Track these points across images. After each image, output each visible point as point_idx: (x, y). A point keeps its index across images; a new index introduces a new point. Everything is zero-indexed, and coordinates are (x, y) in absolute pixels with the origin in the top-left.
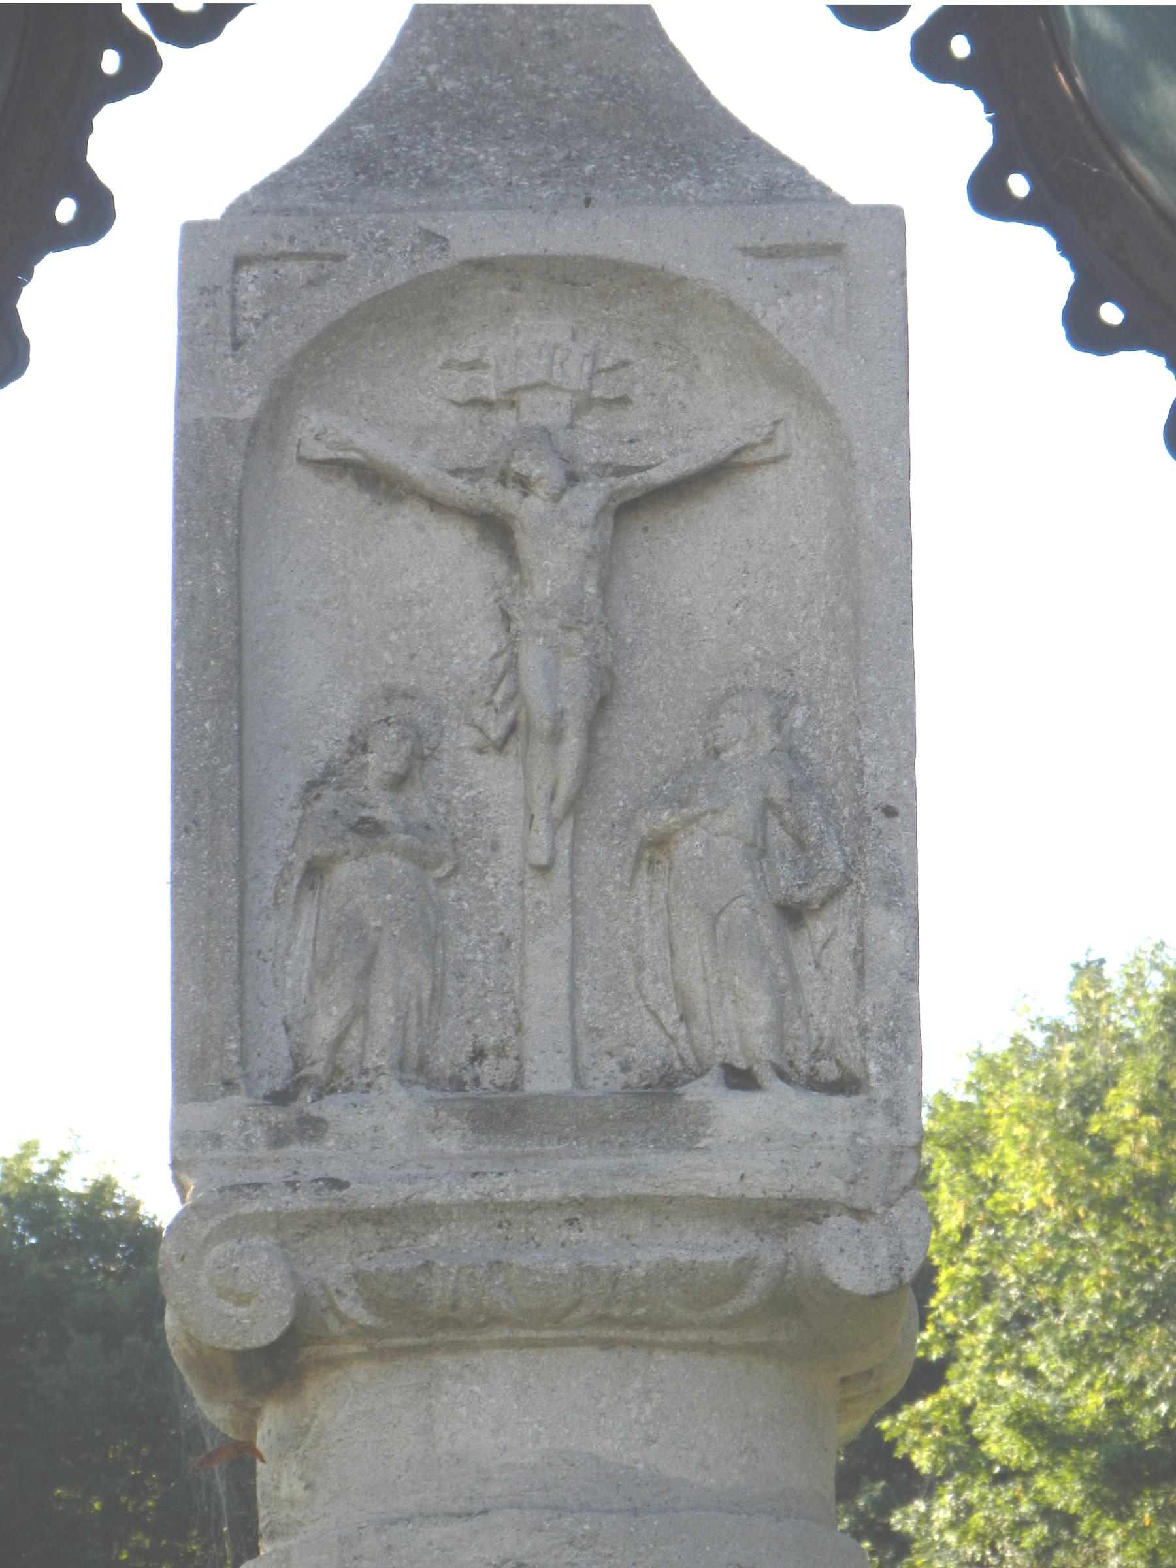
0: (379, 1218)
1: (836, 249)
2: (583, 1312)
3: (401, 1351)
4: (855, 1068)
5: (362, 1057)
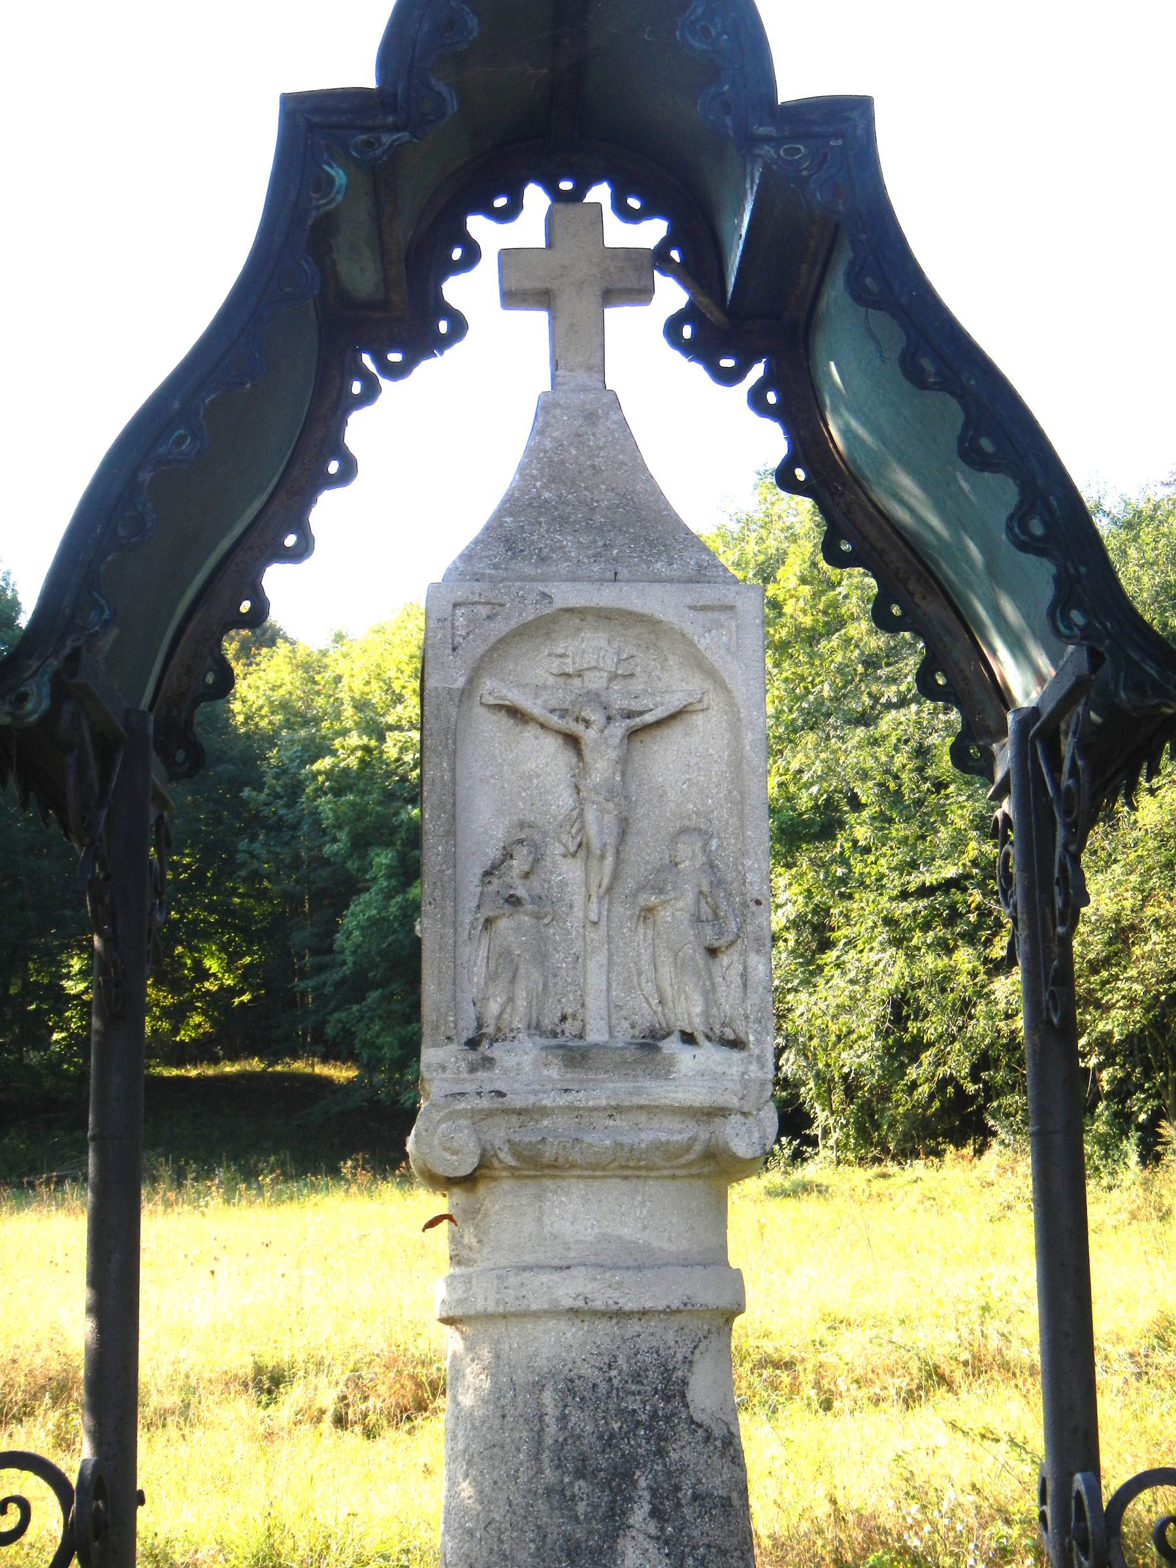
0: (520, 1112)
1: (732, 608)
2: (616, 1164)
3: (526, 1177)
4: (742, 1035)
5: (510, 1022)
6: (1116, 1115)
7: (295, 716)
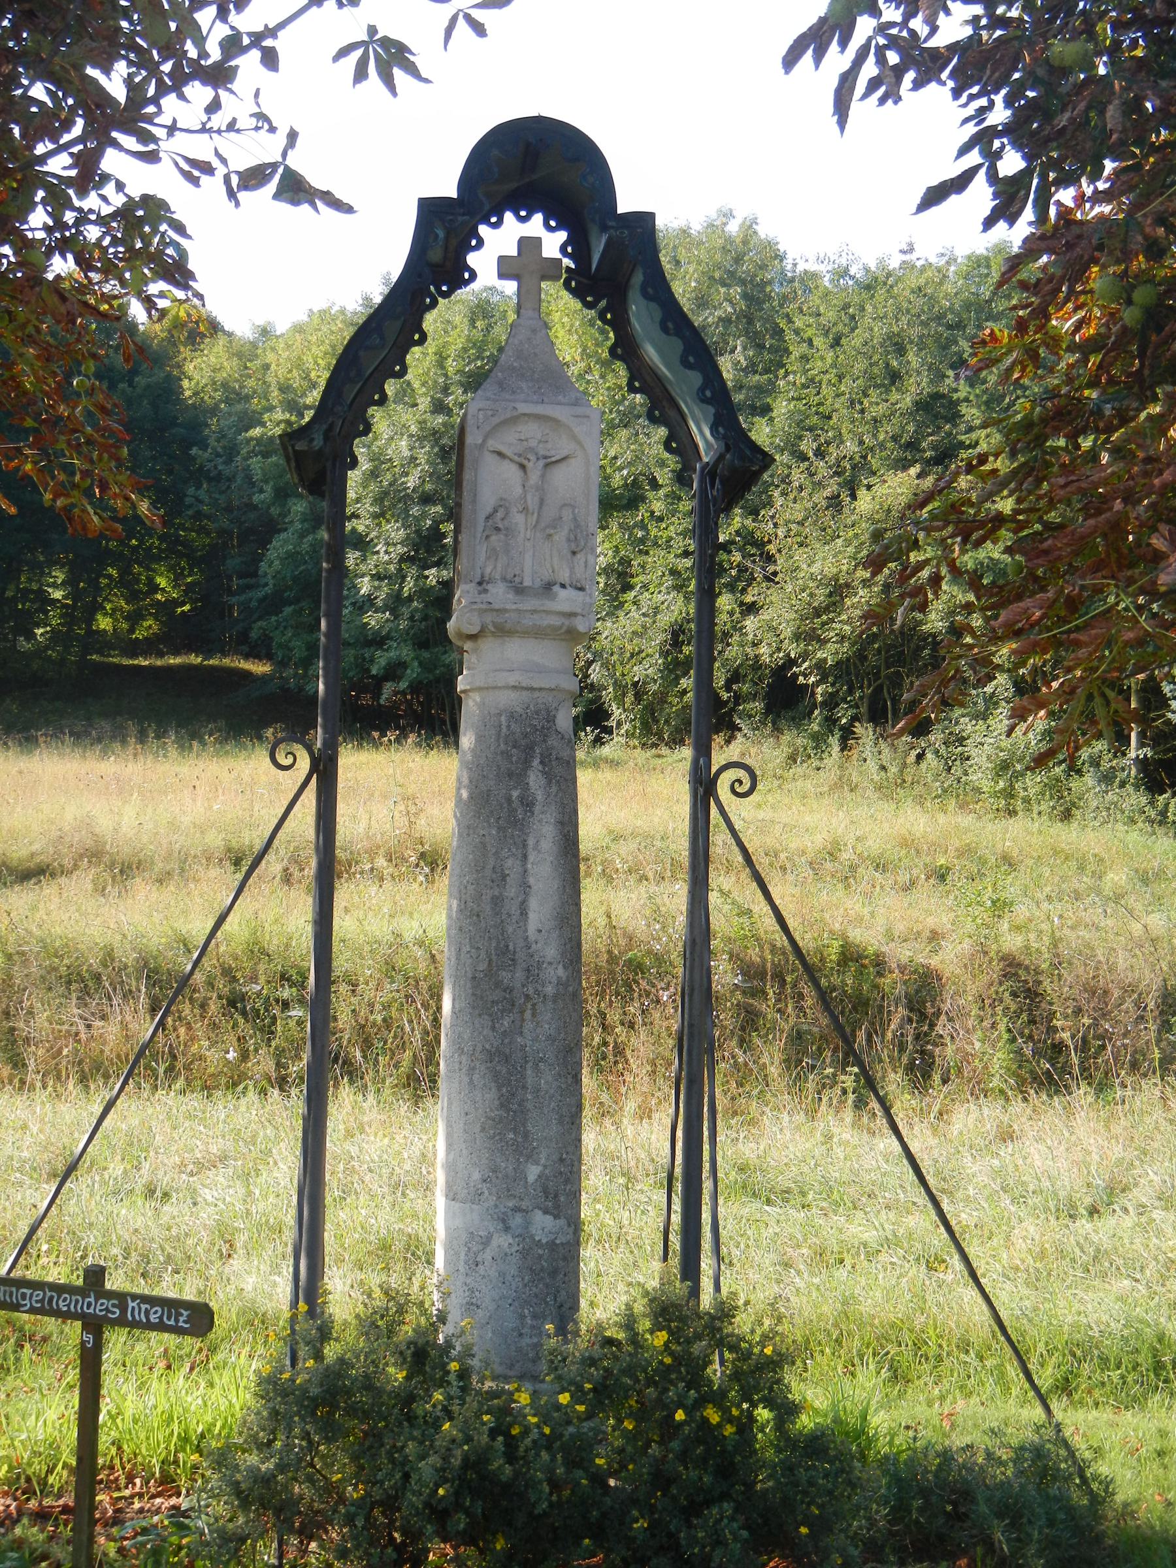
6: (827, 719)
7: (234, 395)
